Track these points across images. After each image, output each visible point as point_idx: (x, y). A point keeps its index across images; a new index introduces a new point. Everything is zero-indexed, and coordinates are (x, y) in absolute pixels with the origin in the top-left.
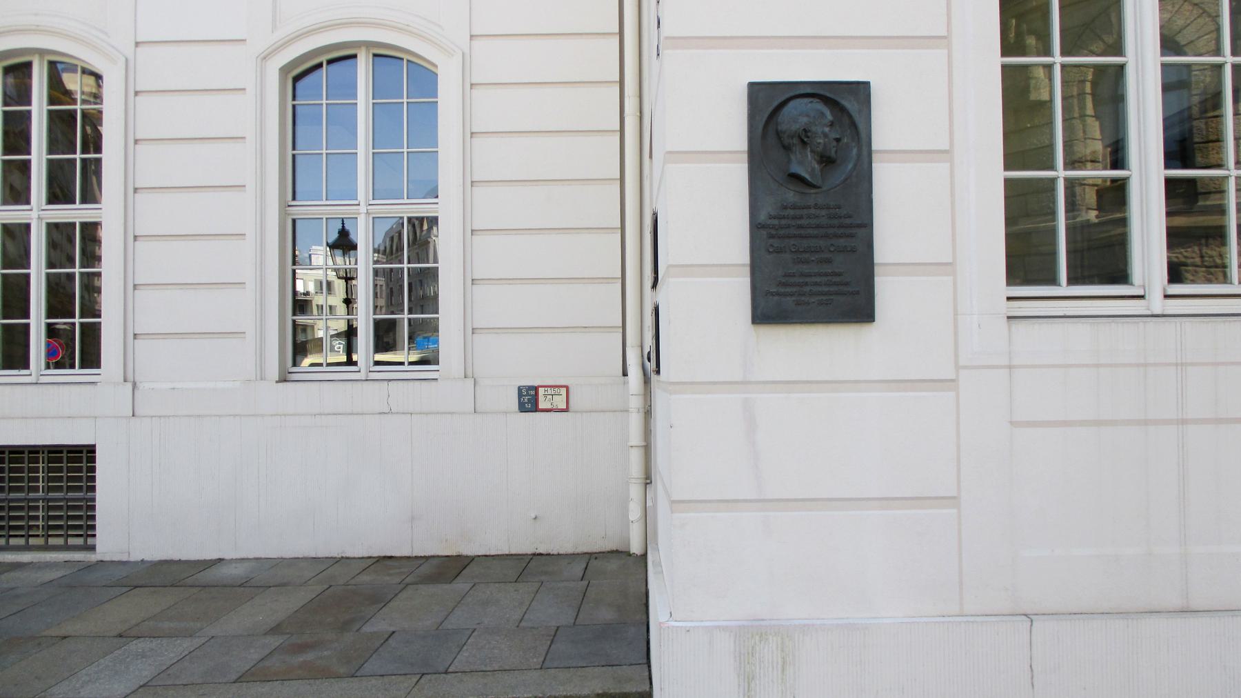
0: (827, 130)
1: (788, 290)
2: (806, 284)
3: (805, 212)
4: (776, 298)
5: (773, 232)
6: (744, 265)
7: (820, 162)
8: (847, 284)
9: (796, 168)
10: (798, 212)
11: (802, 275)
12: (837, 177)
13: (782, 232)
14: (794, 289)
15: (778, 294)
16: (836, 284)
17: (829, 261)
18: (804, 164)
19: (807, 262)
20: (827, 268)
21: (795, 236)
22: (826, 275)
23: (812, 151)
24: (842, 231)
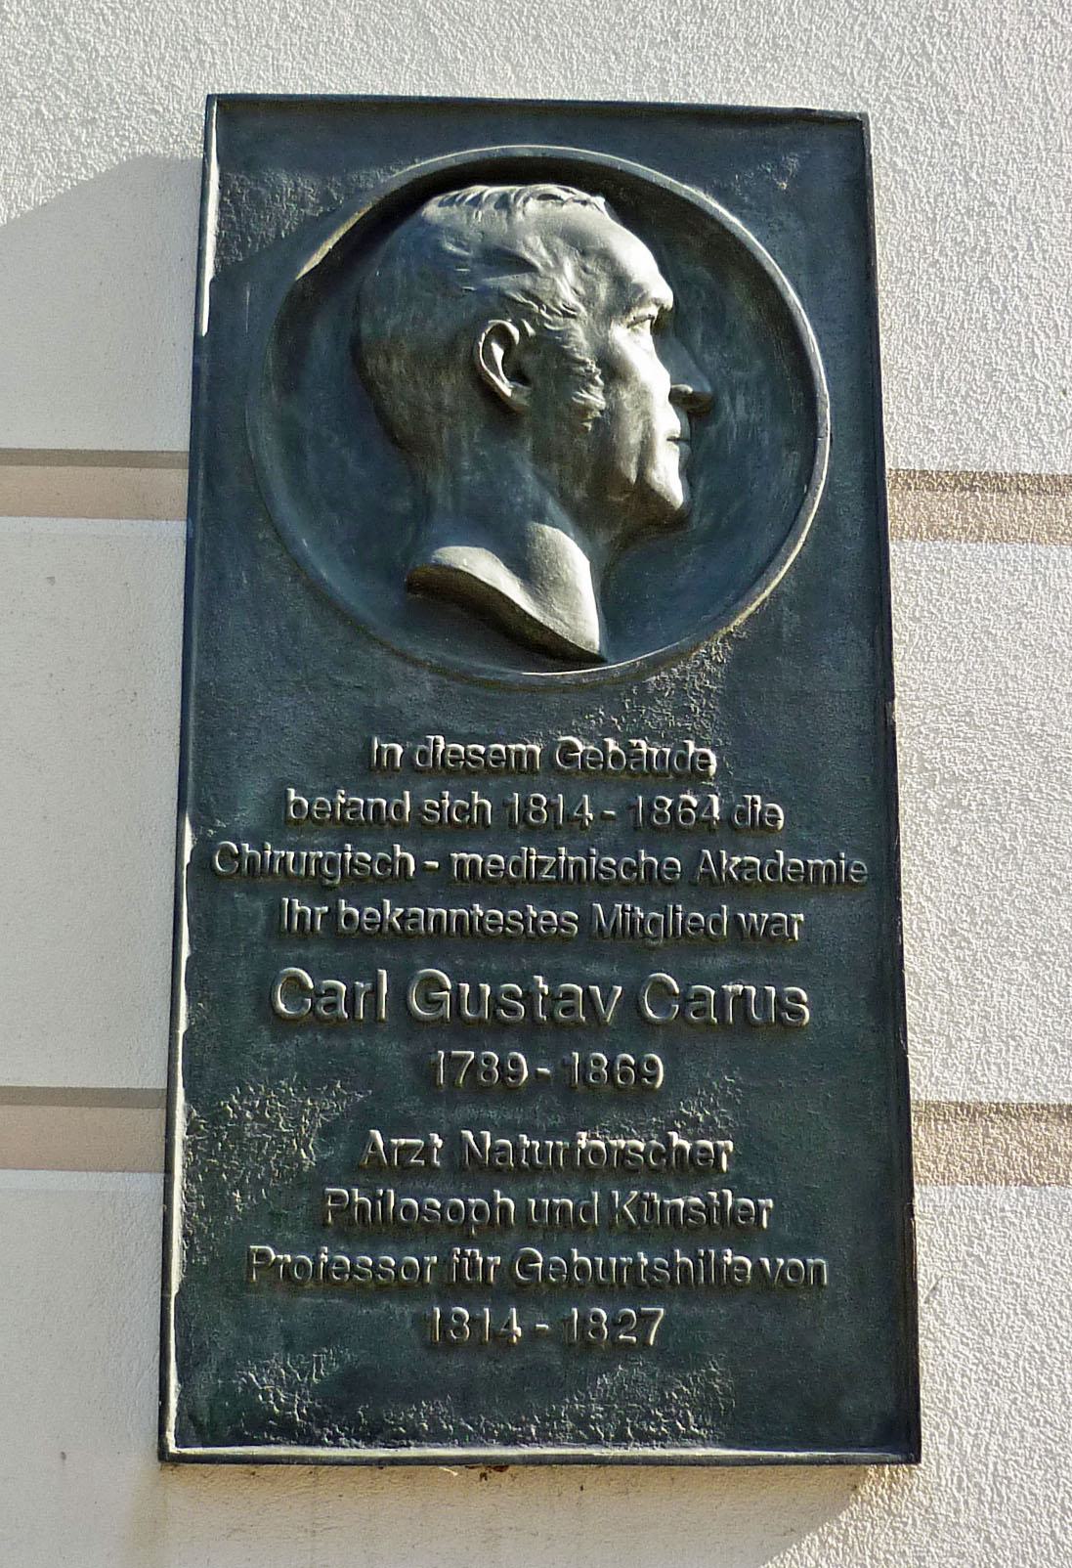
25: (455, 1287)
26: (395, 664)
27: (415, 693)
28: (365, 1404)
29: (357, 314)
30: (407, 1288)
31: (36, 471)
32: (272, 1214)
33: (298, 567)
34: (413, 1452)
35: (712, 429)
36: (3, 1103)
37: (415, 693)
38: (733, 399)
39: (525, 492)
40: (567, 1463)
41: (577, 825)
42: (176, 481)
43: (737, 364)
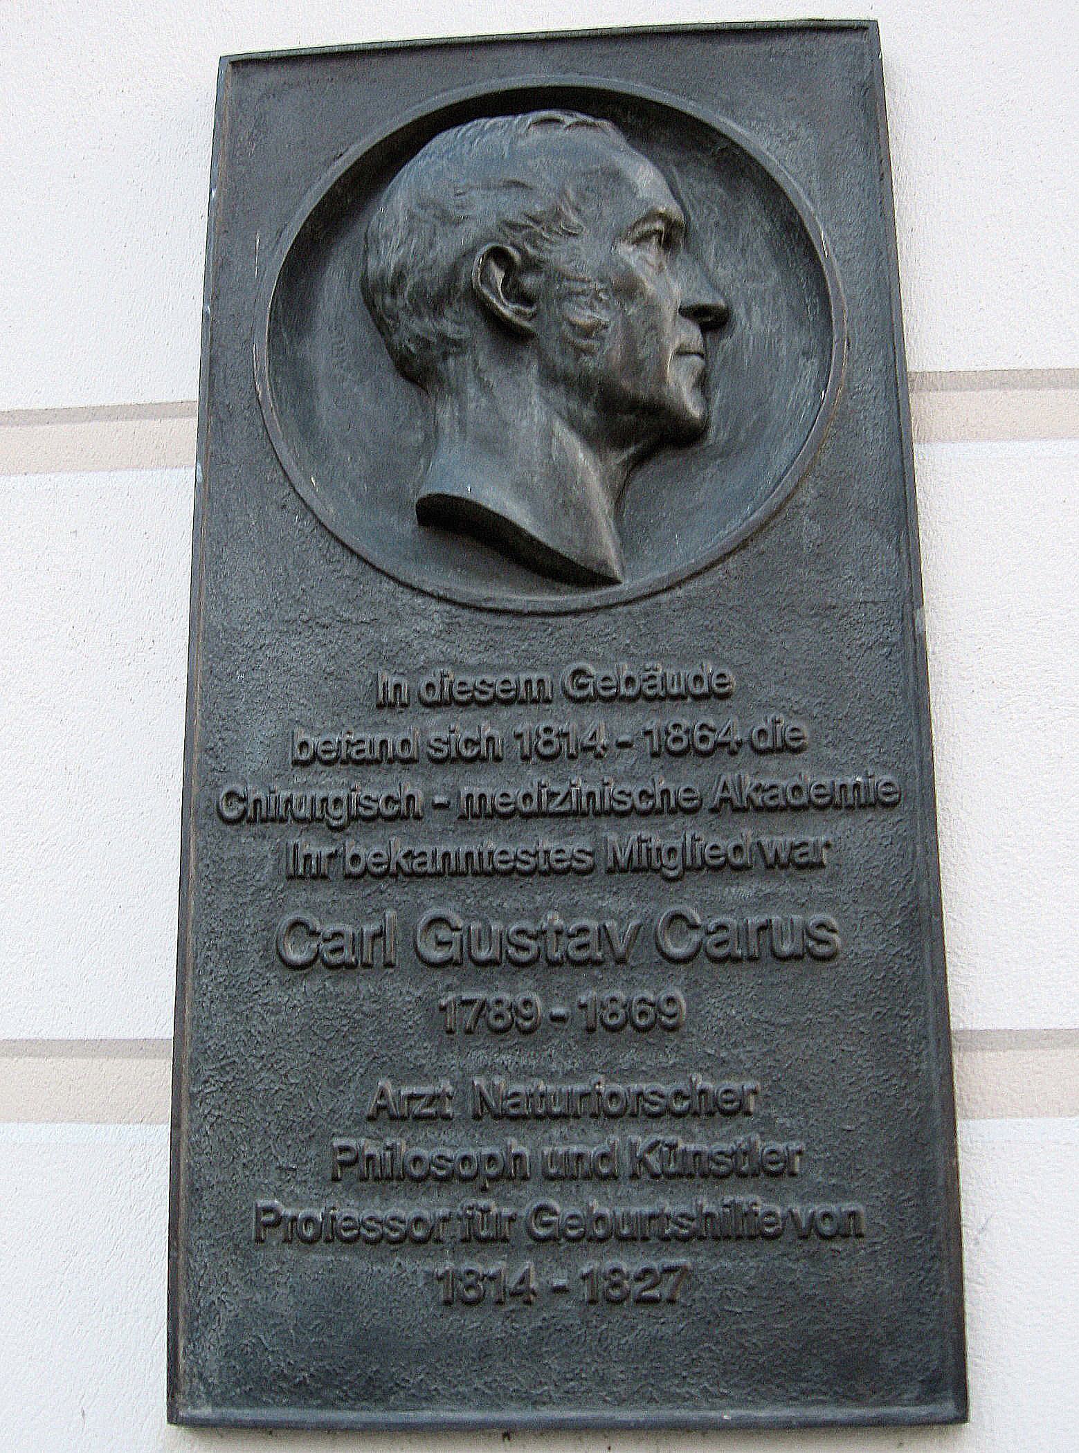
1: (403, 1208)
2: (512, 1172)
3: (526, 721)
4: (319, 1259)
5: (316, 846)
6: (140, 1048)
7: (601, 438)
8: (774, 1172)
12: (702, 512)
13: (365, 847)
14: (431, 1206)
15: (331, 1234)
16: (697, 1171)
17: (656, 1026)
18: (519, 449)
19: (519, 1028)
20: (651, 1074)
24: (746, 832)
27: (423, 625)
28: (349, 1372)
31: (63, 429)
32: (280, 1167)
34: (427, 1415)
35: (727, 342)
36: (3, 1055)
37: (423, 625)
41: (591, 755)
42: (188, 428)
43: (753, 276)
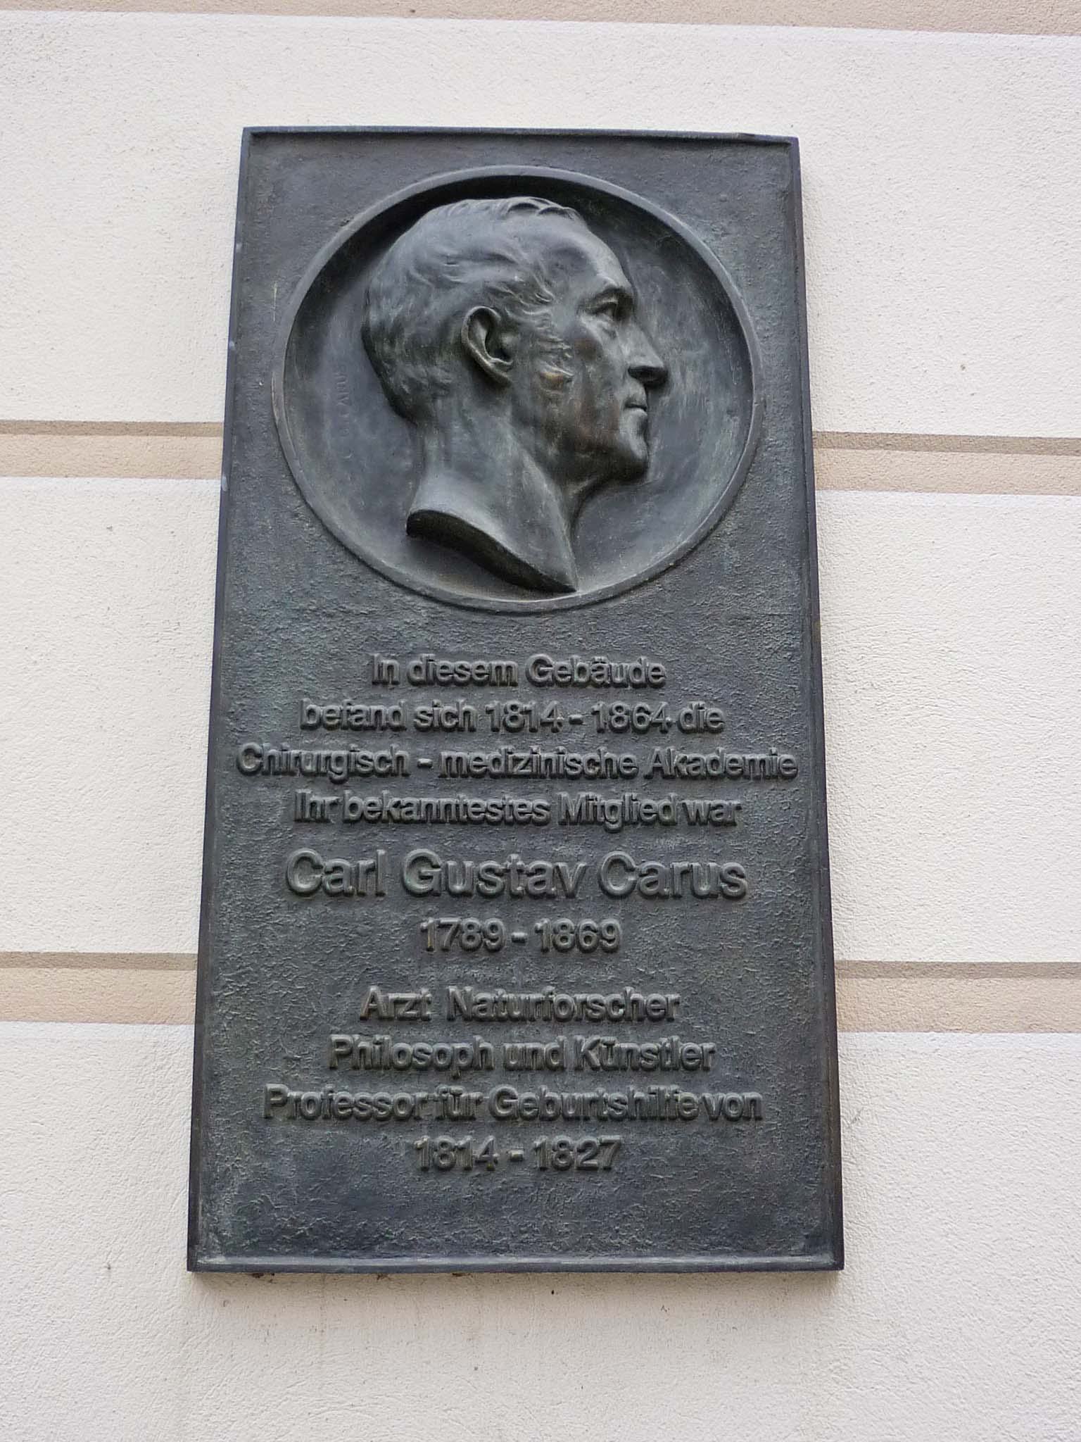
0: (595, 326)
2: (479, 1064)
3: (496, 701)
6: (843, 976)
7: (561, 473)
9: (442, 495)
10: (447, 704)
11: (462, 1016)
12: (652, 540)
13: (363, 799)
18: (484, 481)
19: (488, 949)
21: (432, 819)
22: (588, 1017)
23: (522, 419)
25: (456, 1117)
26: (397, 595)
29: (367, 306)
30: (407, 1118)
31: (101, 440)
33: (621, 592)
35: (666, 399)
38: (683, 374)
39: (506, 450)
40: (813, 1269)
42: (214, 446)
43: (687, 345)
